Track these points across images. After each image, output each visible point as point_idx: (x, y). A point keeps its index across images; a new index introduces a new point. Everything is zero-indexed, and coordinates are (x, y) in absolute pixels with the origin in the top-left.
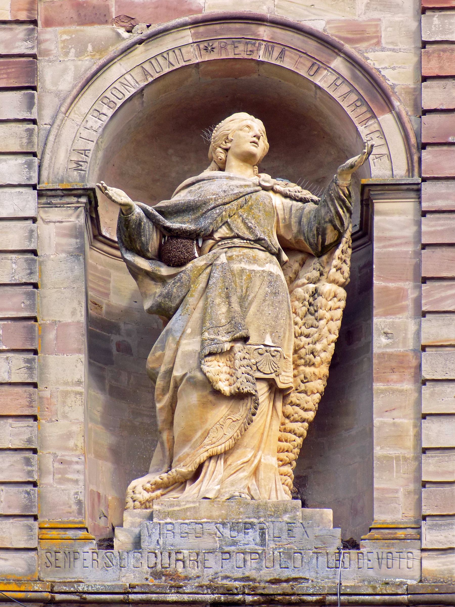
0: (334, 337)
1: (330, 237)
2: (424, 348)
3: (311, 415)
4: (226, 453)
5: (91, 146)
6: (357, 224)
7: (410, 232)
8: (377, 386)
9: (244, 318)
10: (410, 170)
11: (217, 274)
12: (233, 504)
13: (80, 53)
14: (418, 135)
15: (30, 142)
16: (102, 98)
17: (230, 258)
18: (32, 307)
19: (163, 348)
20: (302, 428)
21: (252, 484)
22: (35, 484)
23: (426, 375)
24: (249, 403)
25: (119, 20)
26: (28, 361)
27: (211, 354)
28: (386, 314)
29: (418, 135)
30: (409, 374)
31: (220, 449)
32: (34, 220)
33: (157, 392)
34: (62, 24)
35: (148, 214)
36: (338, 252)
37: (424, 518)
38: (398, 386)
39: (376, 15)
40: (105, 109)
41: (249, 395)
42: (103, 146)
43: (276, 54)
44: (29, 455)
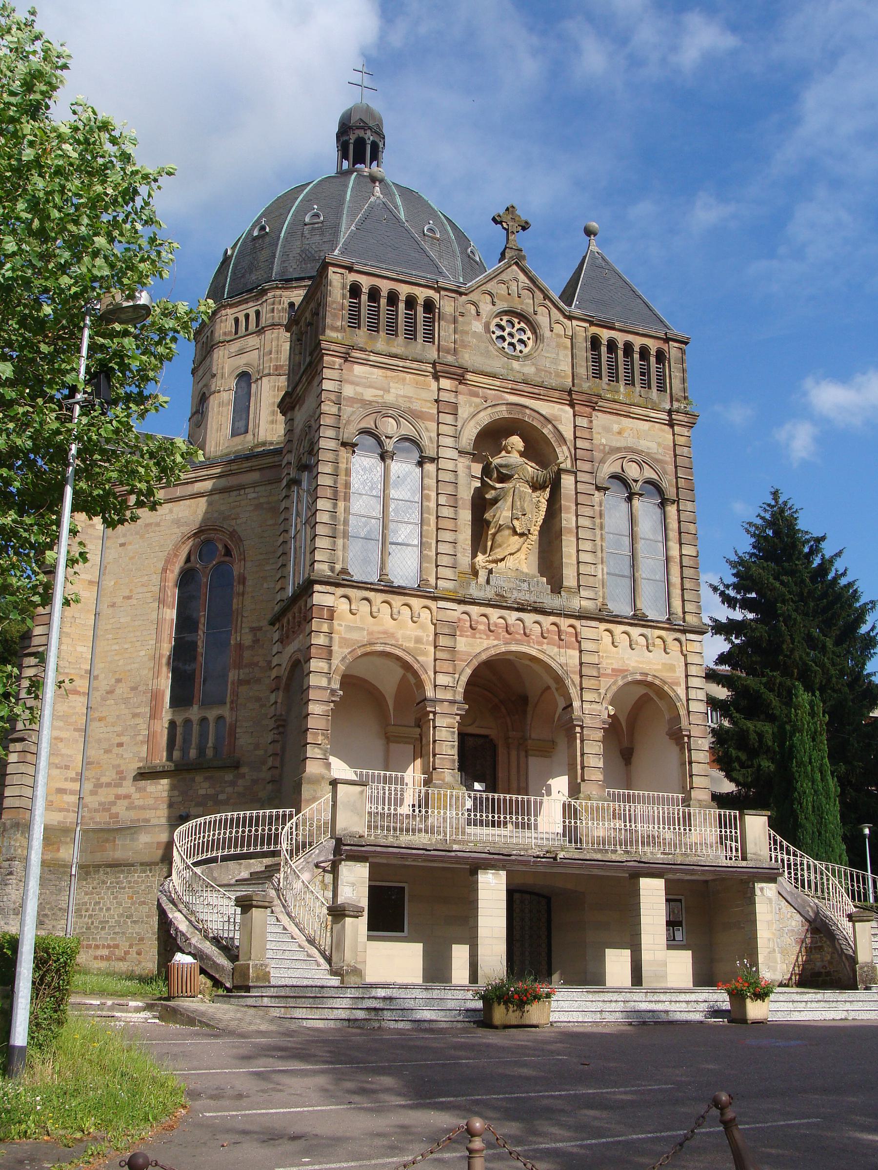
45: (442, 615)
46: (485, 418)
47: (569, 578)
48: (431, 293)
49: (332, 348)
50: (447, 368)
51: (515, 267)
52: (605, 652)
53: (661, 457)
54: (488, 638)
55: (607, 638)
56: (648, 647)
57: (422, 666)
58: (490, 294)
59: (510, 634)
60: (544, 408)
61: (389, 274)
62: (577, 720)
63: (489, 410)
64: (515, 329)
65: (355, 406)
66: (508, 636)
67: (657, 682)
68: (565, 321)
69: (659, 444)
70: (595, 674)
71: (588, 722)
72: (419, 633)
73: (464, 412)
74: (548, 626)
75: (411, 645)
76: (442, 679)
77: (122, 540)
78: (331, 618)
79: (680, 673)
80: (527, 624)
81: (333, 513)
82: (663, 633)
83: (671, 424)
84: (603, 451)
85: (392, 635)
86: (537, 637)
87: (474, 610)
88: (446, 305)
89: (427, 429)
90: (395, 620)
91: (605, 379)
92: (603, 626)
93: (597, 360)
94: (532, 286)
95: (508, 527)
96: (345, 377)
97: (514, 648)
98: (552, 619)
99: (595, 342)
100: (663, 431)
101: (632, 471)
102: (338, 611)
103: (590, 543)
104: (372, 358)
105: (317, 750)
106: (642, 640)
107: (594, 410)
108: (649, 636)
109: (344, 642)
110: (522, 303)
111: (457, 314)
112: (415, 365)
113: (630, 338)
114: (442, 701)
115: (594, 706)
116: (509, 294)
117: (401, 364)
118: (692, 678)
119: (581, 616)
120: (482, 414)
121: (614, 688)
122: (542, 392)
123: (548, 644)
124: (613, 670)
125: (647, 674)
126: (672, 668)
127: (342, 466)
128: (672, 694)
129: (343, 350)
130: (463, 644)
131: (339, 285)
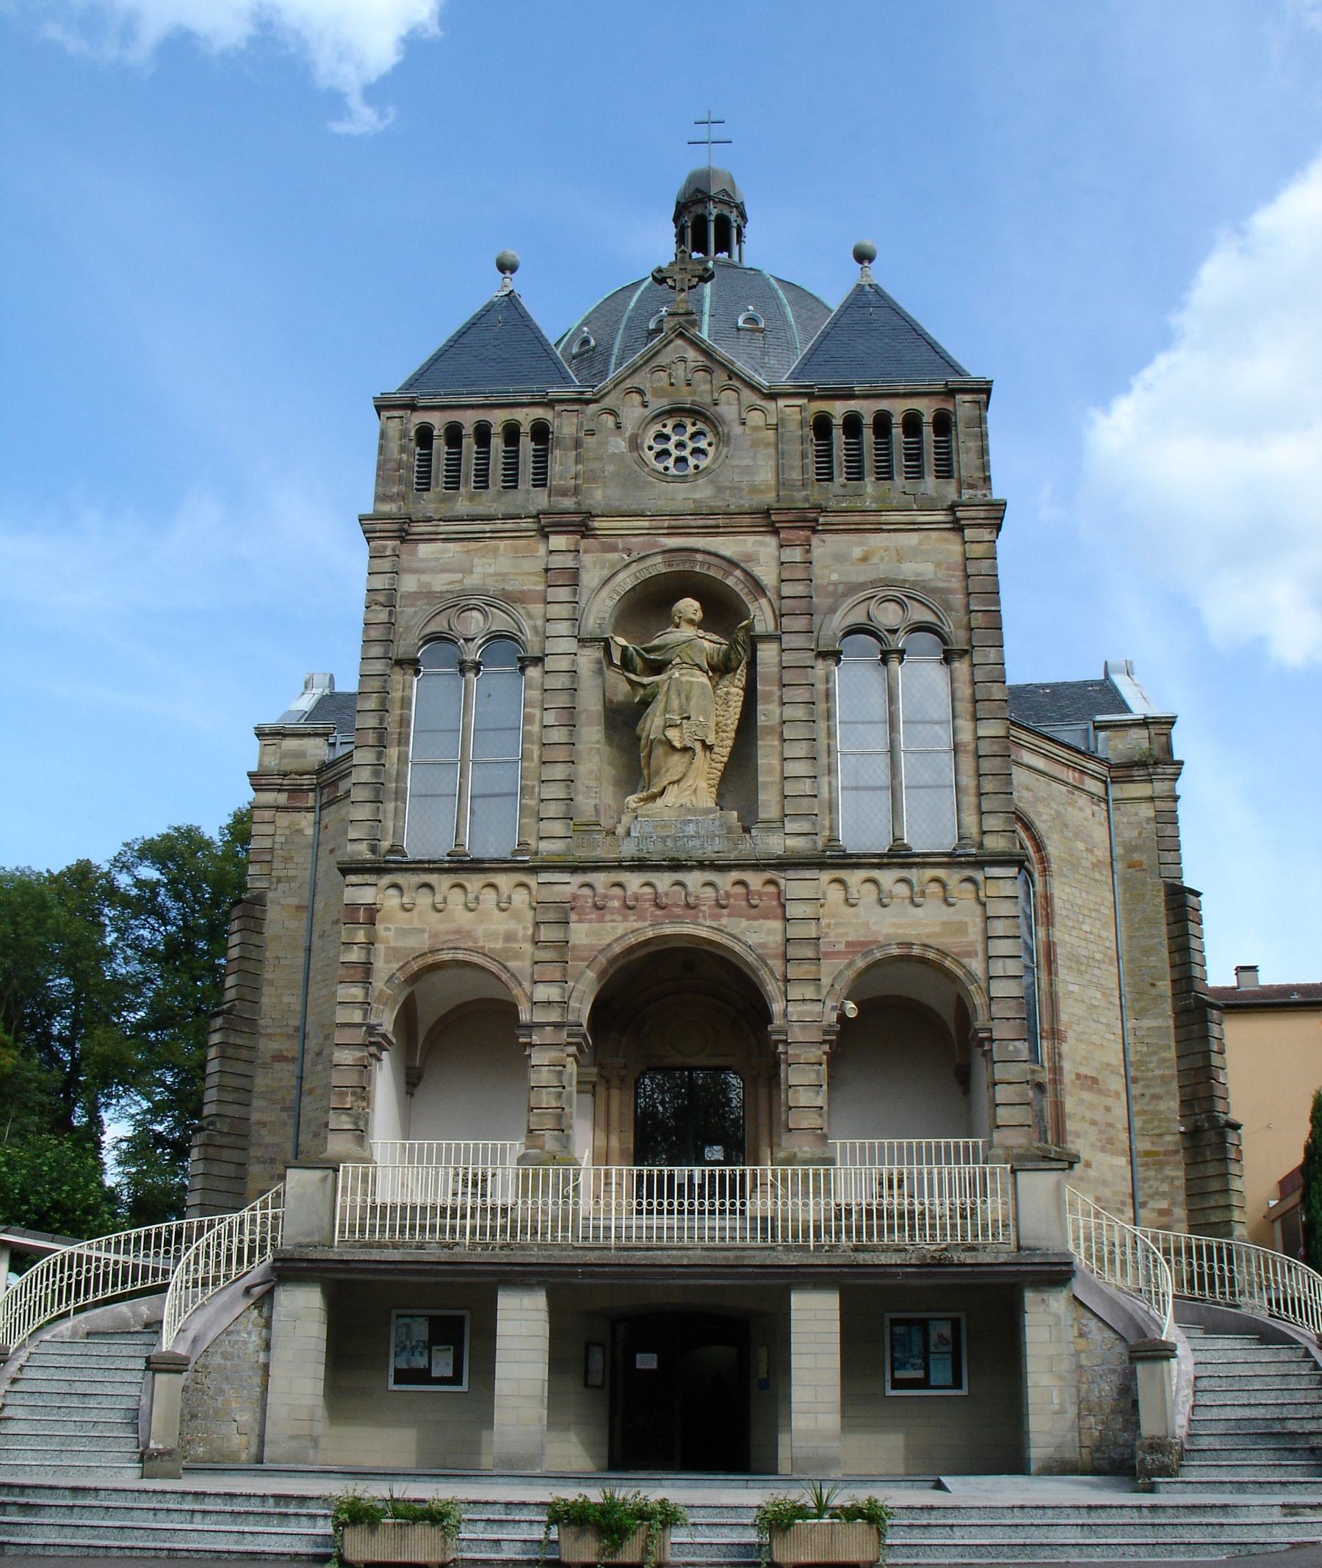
0: (738, 717)
1: (734, 664)
2: (784, 722)
3: (725, 759)
4: (678, 781)
5: (607, 615)
6: (1040, 1298)
7: (776, 660)
8: (759, 743)
9: (688, 705)
10: (776, 628)
11: (673, 683)
12: (682, 809)
13: (603, 567)
14: (780, 610)
15: (574, 613)
16: (614, 591)
17: (681, 675)
18: (573, 701)
19: (645, 723)
20: (721, 766)
21: (694, 799)
22: (572, 800)
23: (786, 737)
24: (691, 752)
25: (623, 550)
26: (570, 731)
27: (670, 726)
28: (764, 704)
29: (780, 610)
30: (777, 736)
31: (675, 778)
32: (576, 654)
33: (642, 747)
34: (593, 552)
35: (637, 651)
36: (739, 671)
37: (786, 816)
38: (771, 743)
39: (757, 549)
40: (615, 596)
41: (691, 748)
42: (615, 615)
43: (705, 568)
44: (569, 783)
45: (545, 894)
46: (626, 581)
47: (769, 803)
48: (539, 413)
49: (378, 527)
50: (557, 519)
51: (679, 342)
52: (834, 916)
53: (940, 584)
54: (625, 919)
55: (835, 894)
56: (912, 900)
57: (513, 975)
58: (640, 392)
59: (662, 908)
60: (727, 546)
61: (472, 400)
62: (779, 1032)
63: (634, 567)
64: (688, 435)
65: (419, 603)
66: (660, 912)
67: (931, 955)
68: (763, 403)
69: (938, 565)
70: (810, 954)
71: (796, 1034)
72: (512, 925)
73: (590, 578)
74: (728, 888)
75: (498, 945)
76: (542, 993)
77: (330, 847)
78: (371, 921)
79: (974, 934)
80: (690, 889)
81: (378, 767)
82: (940, 873)
83: (958, 527)
84: (833, 594)
85: (468, 934)
86: (710, 907)
87: (600, 879)
88: (565, 425)
89: (529, 615)
90: (471, 910)
91: (840, 479)
92: (826, 876)
93: (825, 454)
94: (709, 364)
95: (661, 742)
96: (406, 565)
97: (668, 930)
98: (735, 875)
99: (822, 426)
100: (947, 541)
101: (889, 616)
102: (385, 908)
103: (805, 745)
104: (441, 529)
105: (344, 1118)
106: (902, 890)
107: (814, 531)
108: (914, 881)
109: (393, 953)
110: (694, 393)
111: (582, 434)
112: (510, 525)
113: (884, 405)
114: (542, 1025)
115: (809, 1007)
116: (672, 384)
117: (487, 528)
118: (996, 941)
119: (786, 863)
120: (621, 576)
121: (850, 974)
122: (720, 522)
123: (730, 915)
124: (848, 944)
125: (910, 945)
126: (961, 928)
127: (396, 695)
128: (960, 973)
129: (395, 527)
130: (581, 933)
131: (397, 434)
